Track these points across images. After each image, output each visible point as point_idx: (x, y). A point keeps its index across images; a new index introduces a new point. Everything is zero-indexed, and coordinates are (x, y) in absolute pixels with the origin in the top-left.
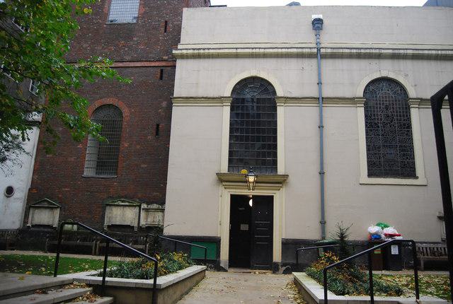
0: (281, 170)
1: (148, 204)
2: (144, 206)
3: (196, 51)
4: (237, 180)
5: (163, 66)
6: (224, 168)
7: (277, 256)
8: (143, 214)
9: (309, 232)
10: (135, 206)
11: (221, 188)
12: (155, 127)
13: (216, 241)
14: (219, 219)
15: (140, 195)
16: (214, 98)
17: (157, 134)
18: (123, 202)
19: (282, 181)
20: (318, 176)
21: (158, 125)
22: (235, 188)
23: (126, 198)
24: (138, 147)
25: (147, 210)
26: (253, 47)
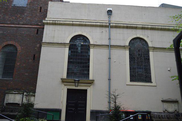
0: (91, 77)
2: (25, 94)
6: (65, 76)
13: (59, 111)
17: (34, 59)
18: (15, 91)
20: (107, 81)
21: (34, 55)
22: (69, 86)
24: (24, 65)
25: (26, 96)
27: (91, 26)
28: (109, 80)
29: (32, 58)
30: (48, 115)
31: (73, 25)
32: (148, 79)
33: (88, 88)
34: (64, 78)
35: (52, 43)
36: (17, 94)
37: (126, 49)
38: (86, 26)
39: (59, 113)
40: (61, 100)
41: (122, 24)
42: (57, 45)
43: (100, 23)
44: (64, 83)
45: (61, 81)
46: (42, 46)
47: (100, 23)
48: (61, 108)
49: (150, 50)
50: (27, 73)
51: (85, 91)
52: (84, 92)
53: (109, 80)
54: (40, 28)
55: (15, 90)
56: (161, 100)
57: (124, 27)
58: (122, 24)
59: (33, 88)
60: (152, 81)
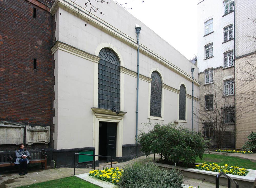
0: (122, 109)
1: (32, 125)
2: (28, 127)
3: (151, 54)
4: (103, 113)
5: (37, 6)
6: (96, 105)
7: (119, 153)
8: (28, 134)
9: (132, 141)
10: (20, 128)
11: (94, 117)
12: (33, 61)
13: (93, 150)
14: (93, 137)
15: (22, 118)
16: (89, 54)
17: (35, 68)
18: (5, 124)
19: (121, 114)
20: (191, 120)
21: (35, 60)
22: (102, 118)
23: (7, 120)
24: (17, 75)
25: (32, 131)
26: (112, 28)
27: (132, 47)
28: (92, 108)
29: (32, 65)
30: (79, 156)
31: (102, 29)
32: (159, 115)
33: (119, 120)
34: (95, 107)
35: (131, 71)
36: (11, 129)
37: (95, 61)
38: (117, 39)
39: (92, 152)
40: (93, 137)
41: (149, 51)
42: (169, 88)
43: (161, 59)
44: (96, 114)
45: (91, 111)
46: (59, 48)
47: (161, 59)
48: (93, 146)
49: (163, 87)
50: (25, 91)
51: (115, 125)
52: (115, 125)
53: (137, 113)
54: (39, 7)
55: (6, 122)
56: (253, 131)
57: (74, 12)
58: (149, 51)
59: (40, 118)
60: (186, 118)
